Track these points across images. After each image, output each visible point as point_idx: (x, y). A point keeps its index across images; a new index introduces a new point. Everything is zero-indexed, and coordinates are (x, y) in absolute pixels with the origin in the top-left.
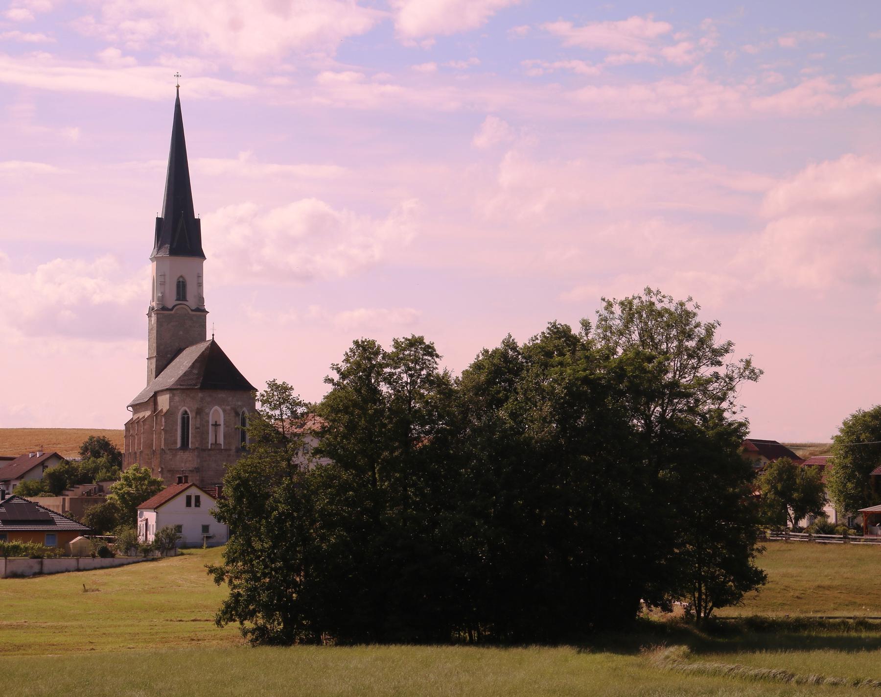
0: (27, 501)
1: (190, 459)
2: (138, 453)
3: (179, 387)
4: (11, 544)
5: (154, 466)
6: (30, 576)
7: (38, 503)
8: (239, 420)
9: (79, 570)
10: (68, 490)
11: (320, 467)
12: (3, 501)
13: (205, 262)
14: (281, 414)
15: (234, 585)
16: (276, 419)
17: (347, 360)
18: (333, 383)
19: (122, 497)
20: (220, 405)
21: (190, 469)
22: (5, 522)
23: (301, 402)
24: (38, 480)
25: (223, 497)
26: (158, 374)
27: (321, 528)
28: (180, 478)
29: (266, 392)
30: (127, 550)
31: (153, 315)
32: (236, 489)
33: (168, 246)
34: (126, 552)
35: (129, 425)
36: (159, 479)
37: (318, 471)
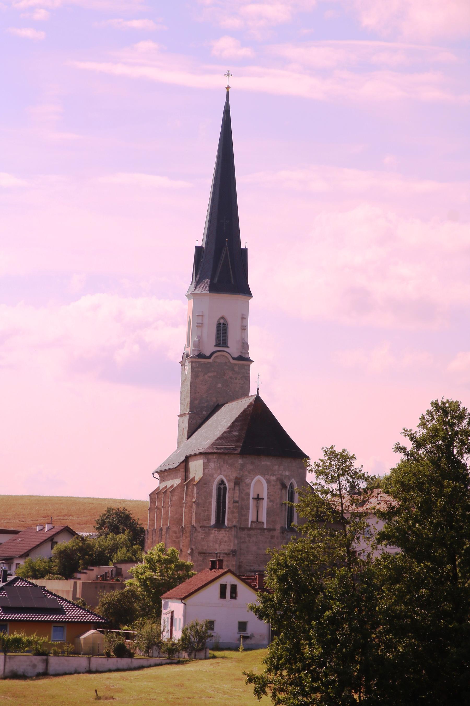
0: (33, 584)
1: (226, 539)
2: (164, 531)
3: (215, 451)
4: (12, 637)
5: (183, 546)
6: (33, 677)
7: (45, 587)
8: (286, 492)
9: (90, 672)
10: (80, 572)
11: (386, 557)
12: (4, 584)
13: (251, 301)
14: (340, 489)
15: (279, 699)
16: (333, 495)
17: (423, 424)
18: (405, 452)
19: (144, 583)
20: (263, 475)
21: (226, 552)
22: (6, 610)
23: (364, 474)
24: (46, 559)
25: (266, 590)
26: (190, 434)
27: (388, 632)
28: (213, 563)
29: (322, 461)
30: (148, 648)
31: (187, 363)
32: (282, 579)
33: (208, 281)
34: (147, 652)
35: (155, 495)
36: (189, 563)
37: (385, 562)
